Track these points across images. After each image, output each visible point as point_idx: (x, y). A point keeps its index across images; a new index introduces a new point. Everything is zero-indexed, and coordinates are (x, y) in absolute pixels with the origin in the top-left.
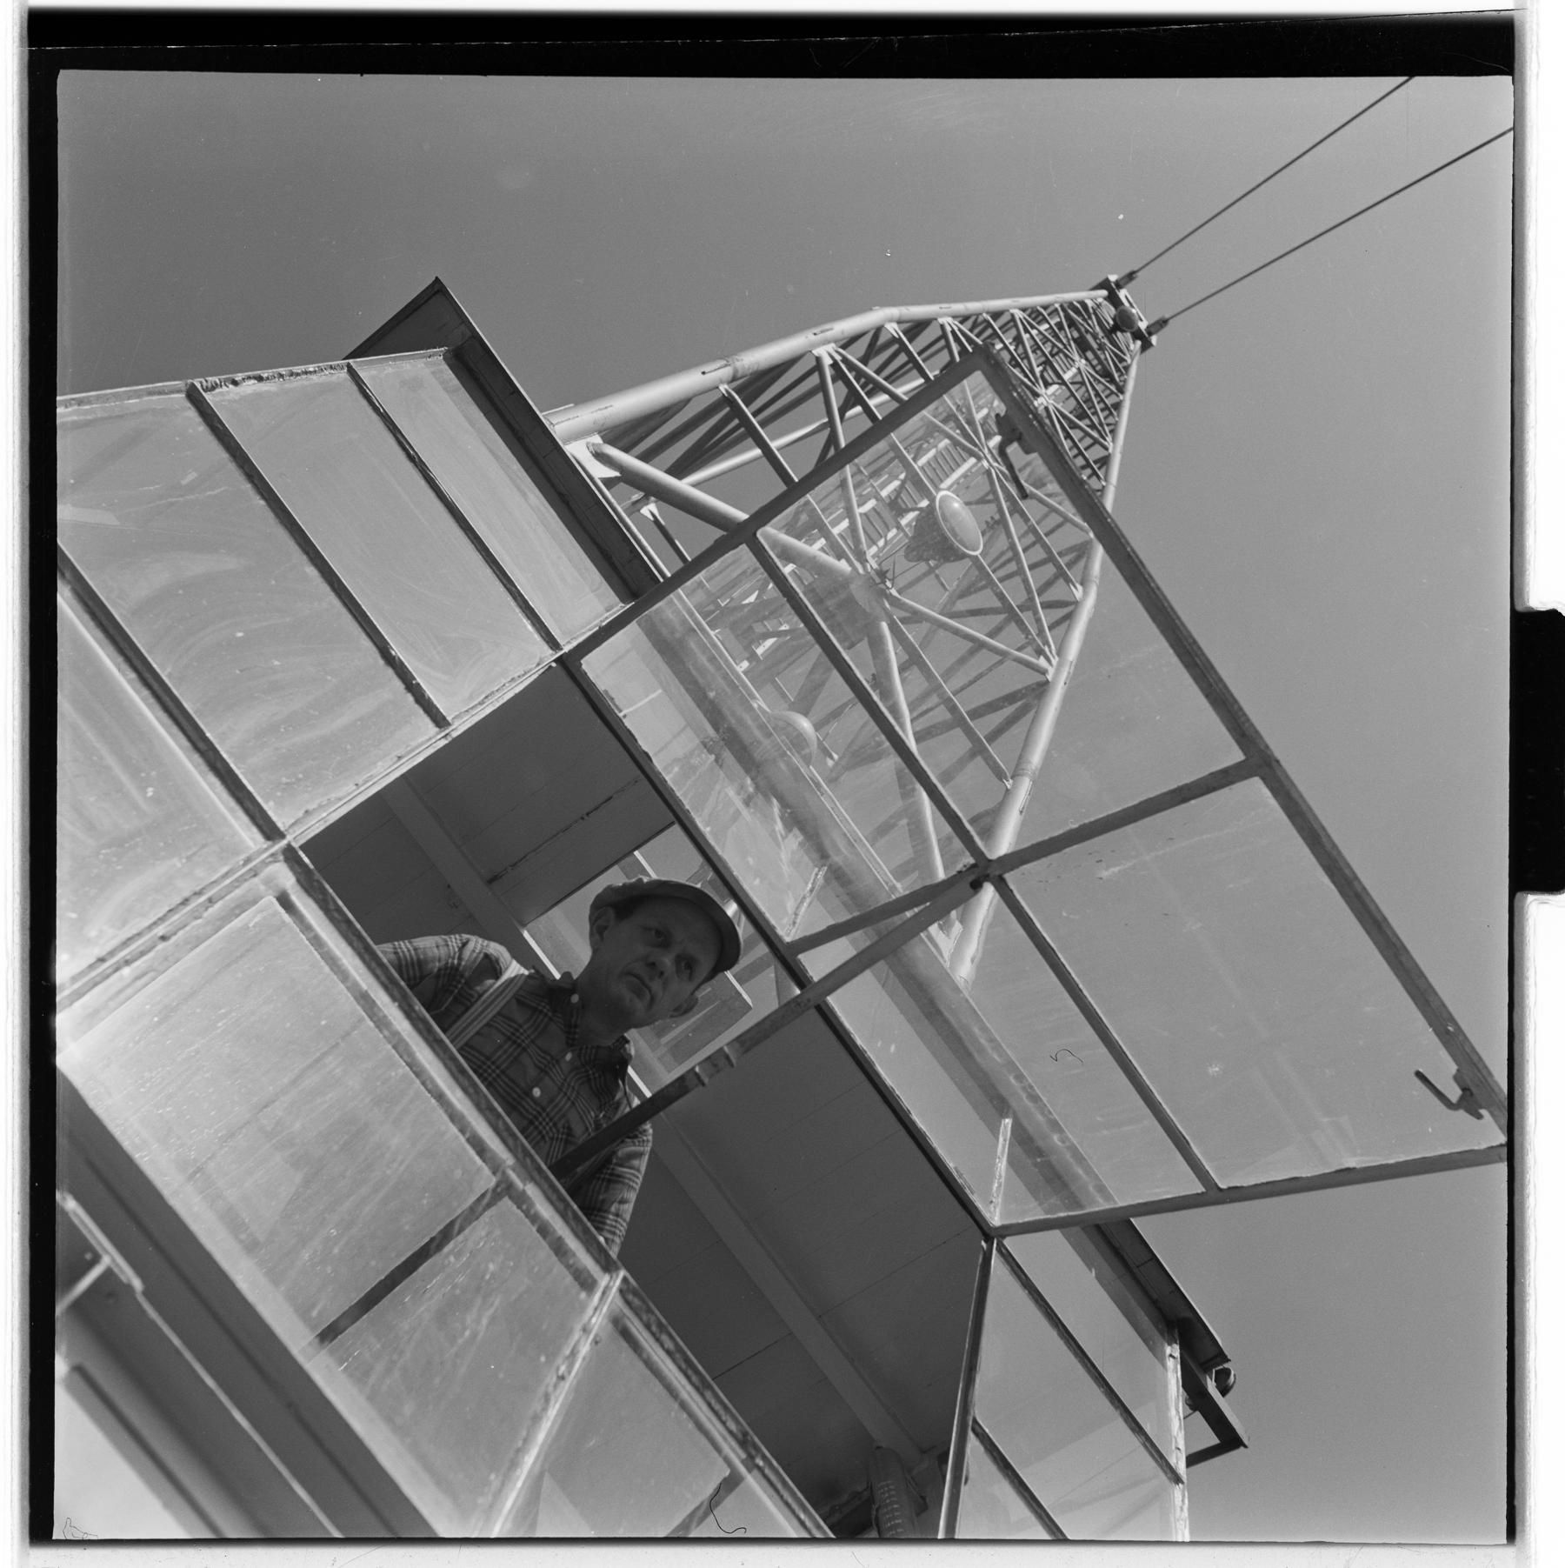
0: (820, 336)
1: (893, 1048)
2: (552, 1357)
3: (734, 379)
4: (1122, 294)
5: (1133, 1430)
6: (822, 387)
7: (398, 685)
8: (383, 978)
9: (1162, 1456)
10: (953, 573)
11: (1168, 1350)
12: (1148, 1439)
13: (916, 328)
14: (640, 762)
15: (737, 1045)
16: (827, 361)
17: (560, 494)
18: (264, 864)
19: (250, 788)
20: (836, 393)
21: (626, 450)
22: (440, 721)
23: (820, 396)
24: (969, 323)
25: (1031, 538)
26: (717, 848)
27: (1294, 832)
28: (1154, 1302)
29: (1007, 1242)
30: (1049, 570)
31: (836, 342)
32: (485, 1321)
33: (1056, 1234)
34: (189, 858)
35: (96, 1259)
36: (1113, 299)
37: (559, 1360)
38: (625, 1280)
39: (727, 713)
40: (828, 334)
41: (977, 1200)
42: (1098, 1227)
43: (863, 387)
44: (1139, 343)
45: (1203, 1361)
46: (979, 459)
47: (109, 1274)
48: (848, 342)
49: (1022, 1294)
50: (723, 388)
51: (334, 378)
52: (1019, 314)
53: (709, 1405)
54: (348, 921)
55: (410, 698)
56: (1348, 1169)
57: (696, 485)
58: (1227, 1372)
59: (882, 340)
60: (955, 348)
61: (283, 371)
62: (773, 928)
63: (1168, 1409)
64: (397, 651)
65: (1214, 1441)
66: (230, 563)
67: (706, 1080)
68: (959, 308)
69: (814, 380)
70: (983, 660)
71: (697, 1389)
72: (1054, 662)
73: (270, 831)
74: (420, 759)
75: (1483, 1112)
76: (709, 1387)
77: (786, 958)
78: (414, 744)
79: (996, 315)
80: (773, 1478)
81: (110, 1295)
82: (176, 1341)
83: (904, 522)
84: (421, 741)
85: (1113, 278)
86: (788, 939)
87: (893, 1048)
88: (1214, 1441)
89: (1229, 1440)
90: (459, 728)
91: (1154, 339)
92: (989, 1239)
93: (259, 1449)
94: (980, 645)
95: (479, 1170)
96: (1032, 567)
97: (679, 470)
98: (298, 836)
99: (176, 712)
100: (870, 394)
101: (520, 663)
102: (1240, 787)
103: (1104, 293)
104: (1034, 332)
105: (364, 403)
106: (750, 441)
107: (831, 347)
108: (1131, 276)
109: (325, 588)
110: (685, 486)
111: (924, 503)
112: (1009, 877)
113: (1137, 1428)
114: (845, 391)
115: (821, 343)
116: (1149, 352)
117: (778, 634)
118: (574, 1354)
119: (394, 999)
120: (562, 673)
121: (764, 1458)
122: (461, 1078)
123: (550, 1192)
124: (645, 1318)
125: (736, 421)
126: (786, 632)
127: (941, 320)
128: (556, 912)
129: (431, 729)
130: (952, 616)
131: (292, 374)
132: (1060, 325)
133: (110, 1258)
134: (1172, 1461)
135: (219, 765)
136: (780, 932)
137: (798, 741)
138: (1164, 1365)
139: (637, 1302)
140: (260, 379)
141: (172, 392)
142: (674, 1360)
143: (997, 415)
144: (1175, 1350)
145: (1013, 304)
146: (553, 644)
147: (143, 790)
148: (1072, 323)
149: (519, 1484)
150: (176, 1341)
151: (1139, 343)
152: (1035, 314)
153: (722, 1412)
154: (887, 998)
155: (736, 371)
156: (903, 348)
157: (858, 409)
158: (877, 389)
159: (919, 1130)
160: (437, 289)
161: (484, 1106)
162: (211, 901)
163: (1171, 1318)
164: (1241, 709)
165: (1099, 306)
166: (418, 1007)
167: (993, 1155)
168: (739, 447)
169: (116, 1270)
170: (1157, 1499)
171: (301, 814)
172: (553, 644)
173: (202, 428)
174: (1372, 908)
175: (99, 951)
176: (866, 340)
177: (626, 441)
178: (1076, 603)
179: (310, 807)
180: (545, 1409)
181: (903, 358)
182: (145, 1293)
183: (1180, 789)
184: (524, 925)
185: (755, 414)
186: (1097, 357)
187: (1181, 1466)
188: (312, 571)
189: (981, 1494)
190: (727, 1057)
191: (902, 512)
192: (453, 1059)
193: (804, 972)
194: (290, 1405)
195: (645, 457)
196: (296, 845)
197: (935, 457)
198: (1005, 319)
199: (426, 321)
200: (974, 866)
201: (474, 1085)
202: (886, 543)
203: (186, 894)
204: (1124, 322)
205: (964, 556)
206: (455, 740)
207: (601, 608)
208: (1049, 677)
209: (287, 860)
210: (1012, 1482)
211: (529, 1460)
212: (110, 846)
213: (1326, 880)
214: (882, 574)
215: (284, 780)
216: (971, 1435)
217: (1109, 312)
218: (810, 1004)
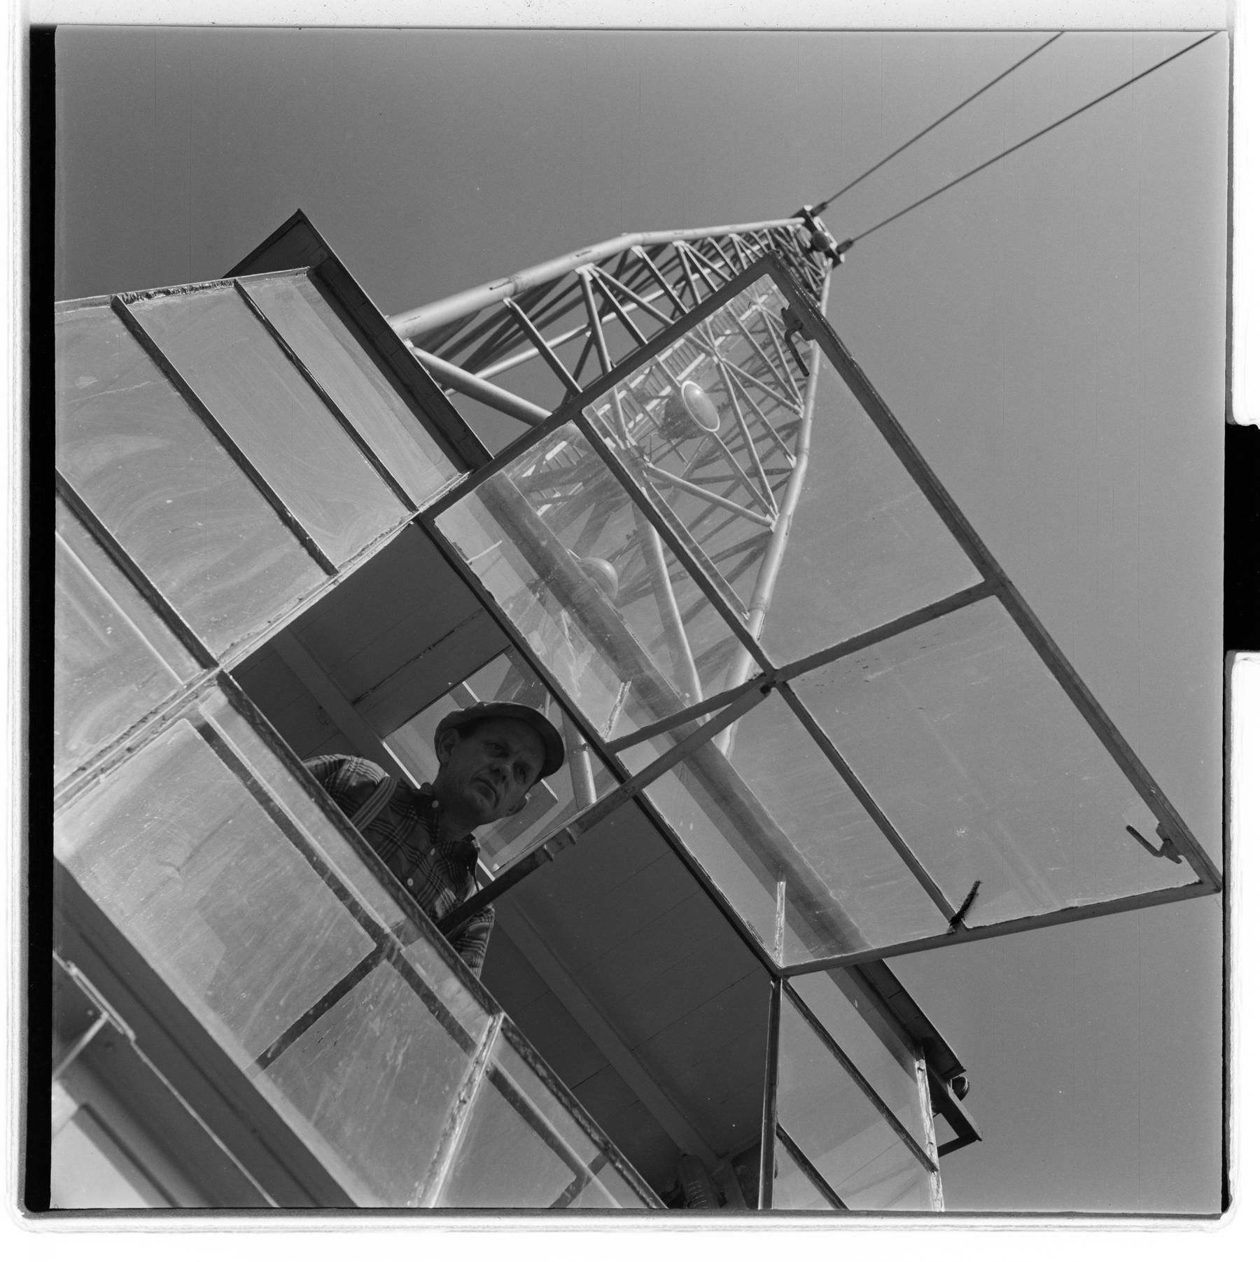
0: (582, 257)
1: (691, 826)
2: (454, 1086)
3: (515, 293)
4: (817, 221)
5: (896, 1130)
6: (584, 298)
7: (295, 541)
8: (302, 779)
9: (920, 1150)
10: (692, 448)
11: (917, 1065)
12: (908, 1136)
13: (656, 250)
14: (484, 600)
15: (577, 826)
16: (588, 278)
17: (406, 386)
18: (203, 687)
19: (188, 625)
20: (595, 302)
21: (431, 351)
22: (329, 570)
23: (583, 305)
24: (698, 245)
25: (752, 417)
26: (549, 668)
27: (1024, 638)
28: (903, 1026)
29: (791, 981)
30: (769, 443)
31: (594, 261)
32: (400, 1058)
33: (823, 975)
34: (144, 684)
35: (97, 1015)
36: (809, 225)
37: (460, 1088)
38: (505, 1019)
39: (558, 558)
40: (588, 256)
41: (764, 946)
42: (856, 967)
43: (616, 296)
44: (831, 260)
45: (945, 1072)
46: (708, 354)
47: (108, 1027)
48: (602, 262)
49: (804, 1024)
50: (507, 301)
51: (224, 292)
52: (736, 238)
53: (577, 1121)
54: (272, 733)
55: (305, 552)
56: (1071, 908)
57: (487, 379)
58: (963, 1080)
59: (630, 259)
60: (744, 262)
61: (185, 286)
62: (595, 732)
63: (920, 1112)
64: (292, 513)
65: (955, 1136)
66: (156, 443)
67: (553, 856)
68: (690, 233)
69: (577, 292)
70: (721, 515)
71: (567, 1108)
72: (776, 517)
73: (206, 661)
74: (316, 600)
75: (1181, 857)
76: (576, 1106)
77: (606, 755)
78: (310, 588)
79: (718, 239)
80: (630, 1177)
81: (108, 1044)
82: (165, 1081)
83: (649, 408)
84: (315, 588)
85: (808, 208)
86: (607, 740)
87: (691, 826)
88: (955, 1136)
89: (966, 1135)
90: (344, 574)
91: (842, 257)
92: (776, 978)
93: (236, 1167)
94: (716, 504)
95: (362, 938)
96: (755, 441)
97: (473, 365)
98: (228, 664)
99: (125, 565)
100: (622, 302)
101: (385, 524)
102: (980, 604)
103: (802, 220)
104: (748, 252)
105: (250, 312)
106: (528, 342)
107: (590, 266)
108: (822, 207)
109: (232, 463)
110: (477, 379)
111: (668, 390)
112: (793, 683)
113: (899, 1128)
114: (601, 300)
115: (582, 263)
116: (838, 268)
117: (553, 501)
118: (471, 1081)
119: (311, 795)
120: (418, 530)
121: (622, 1162)
122: (368, 860)
123: (442, 950)
124: (522, 1051)
125: (516, 326)
126: (559, 499)
127: (675, 244)
128: (408, 726)
129: (324, 577)
130: (698, 482)
131: (192, 289)
132: (768, 246)
133: (108, 1014)
134: (928, 1153)
135: (162, 607)
136: (601, 735)
137: (604, 582)
138: (915, 1080)
139: (515, 1038)
140: (167, 293)
141: (100, 304)
142: (547, 1085)
143: (783, 309)
144: (921, 1064)
145: (731, 230)
146: (411, 506)
147: (104, 628)
148: (778, 245)
149: (439, 1188)
150: (165, 1081)
151: (831, 260)
152: (749, 238)
153: (587, 1125)
154: (683, 788)
155: (516, 287)
156: (646, 266)
157: (613, 315)
158: (626, 299)
159: (717, 892)
160: (299, 219)
161: (386, 881)
162: (164, 718)
163: (915, 1036)
164: (980, 541)
165: (798, 231)
166: (331, 801)
167: (774, 911)
168: (518, 347)
169: (114, 1023)
170: (916, 1187)
171: (228, 646)
172: (411, 506)
173: (126, 334)
174: (1088, 696)
175: (79, 762)
176: (617, 261)
177: (429, 345)
178: (791, 471)
179: (236, 641)
180: (453, 1128)
181: (646, 274)
182: (137, 1042)
183: (932, 607)
184: (383, 738)
185: (532, 320)
186: (798, 272)
187: (935, 1158)
188: (220, 450)
189: (789, 1182)
190: (570, 837)
191: (649, 399)
192: (361, 843)
193: (621, 766)
194: (254, 1131)
195: (446, 357)
196: (226, 671)
197: (671, 355)
198: (724, 242)
199: (292, 245)
200: (762, 675)
201: (378, 863)
202: (635, 425)
203: (145, 714)
204: (819, 243)
205: (701, 432)
206: (341, 584)
207: (442, 478)
208: (773, 528)
209: (220, 684)
210: (810, 1175)
211: (445, 1170)
212: (82, 676)
213: (1051, 676)
214: (641, 450)
215: (213, 619)
216: (776, 1138)
217: (806, 237)
218: (629, 791)
